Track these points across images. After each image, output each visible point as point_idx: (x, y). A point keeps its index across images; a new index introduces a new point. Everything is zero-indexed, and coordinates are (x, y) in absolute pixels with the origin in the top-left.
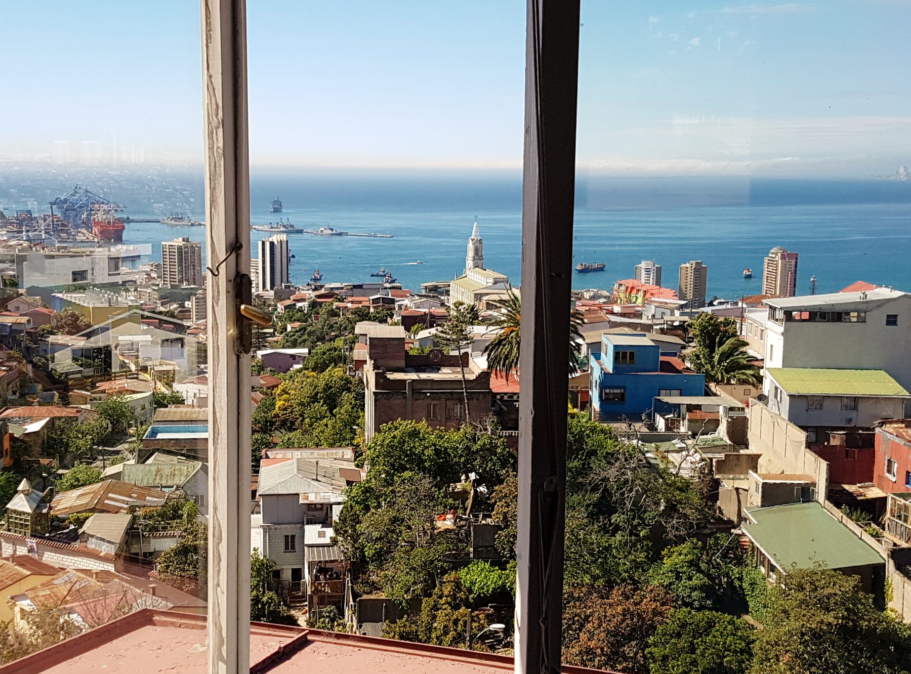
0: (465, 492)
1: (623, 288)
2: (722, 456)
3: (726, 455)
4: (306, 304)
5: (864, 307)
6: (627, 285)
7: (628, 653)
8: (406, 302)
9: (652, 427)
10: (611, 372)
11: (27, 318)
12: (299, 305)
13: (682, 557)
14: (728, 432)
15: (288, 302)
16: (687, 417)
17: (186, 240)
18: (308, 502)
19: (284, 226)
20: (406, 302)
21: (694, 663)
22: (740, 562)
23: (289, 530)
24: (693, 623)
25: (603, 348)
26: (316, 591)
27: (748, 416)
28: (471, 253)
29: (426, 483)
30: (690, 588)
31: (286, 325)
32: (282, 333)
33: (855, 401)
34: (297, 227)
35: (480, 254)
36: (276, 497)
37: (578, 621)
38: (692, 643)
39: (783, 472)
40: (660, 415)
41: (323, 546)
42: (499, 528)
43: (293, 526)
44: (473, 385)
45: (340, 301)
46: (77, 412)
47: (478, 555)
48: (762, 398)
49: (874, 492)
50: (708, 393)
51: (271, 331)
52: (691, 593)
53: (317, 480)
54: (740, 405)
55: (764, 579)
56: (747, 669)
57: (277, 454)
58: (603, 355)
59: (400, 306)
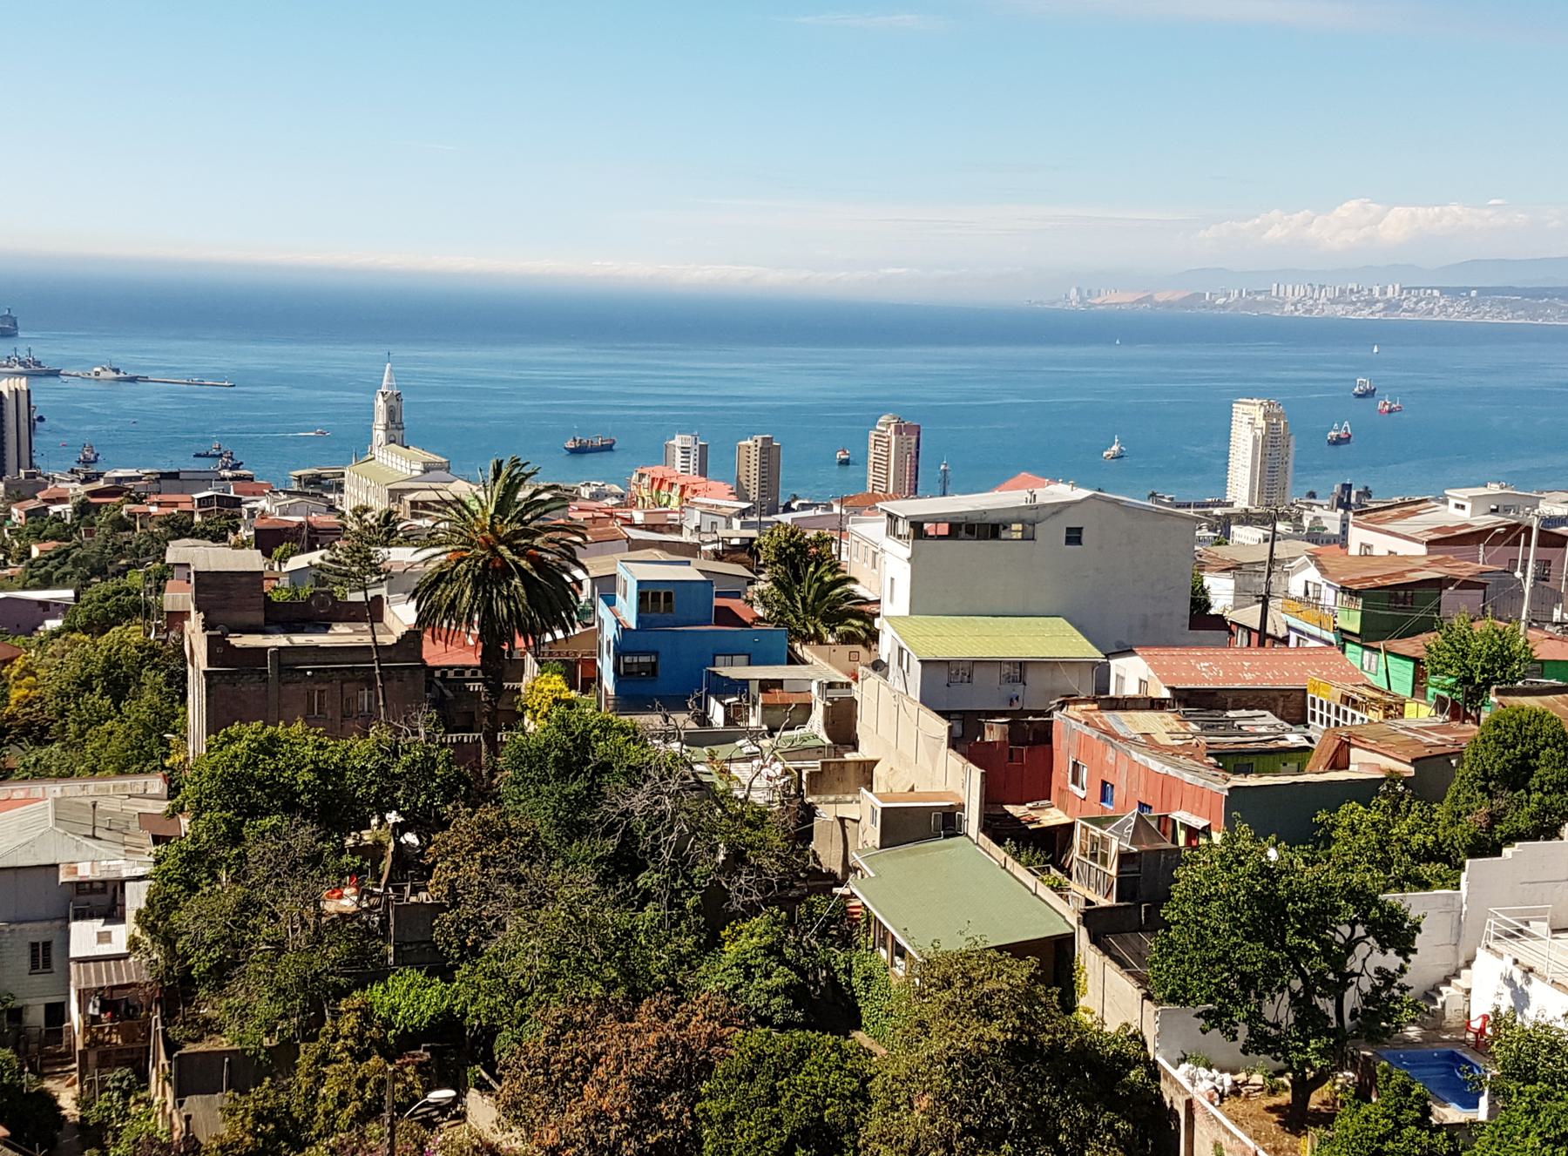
0: (379, 846)
1: (646, 481)
2: (817, 765)
3: (823, 763)
4: (68, 507)
5: (1029, 515)
6: (653, 475)
7: (667, 1114)
8: (263, 504)
9: (703, 719)
10: (634, 627)
12: (54, 509)
13: (755, 939)
14: (826, 724)
15: (32, 504)
16: (761, 701)
18: (77, 879)
19: (22, 364)
20: (263, 504)
21: (777, 1121)
22: (847, 942)
23: (37, 932)
24: (774, 1054)
25: (620, 585)
26: (93, 1043)
27: (857, 697)
28: (381, 419)
29: (305, 836)
30: (768, 992)
31: (29, 547)
32: (20, 561)
34: (47, 366)
36: (11, 872)
37: (581, 1063)
38: (773, 1088)
40: (717, 699)
41: (107, 958)
42: (439, 908)
43: (47, 924)
44: (392, 654)
45: (135, 502)
47: (403, 959)
48: (878, 666)
49: (1052, 817)
50: (793, 660)
52: (769, 1000)
53: (94, 837)
54: (845, 679)
55: (886, 969)
56: (862, 1124)
57: (13, 791)
58: (619, 597)
59: (252, 512)
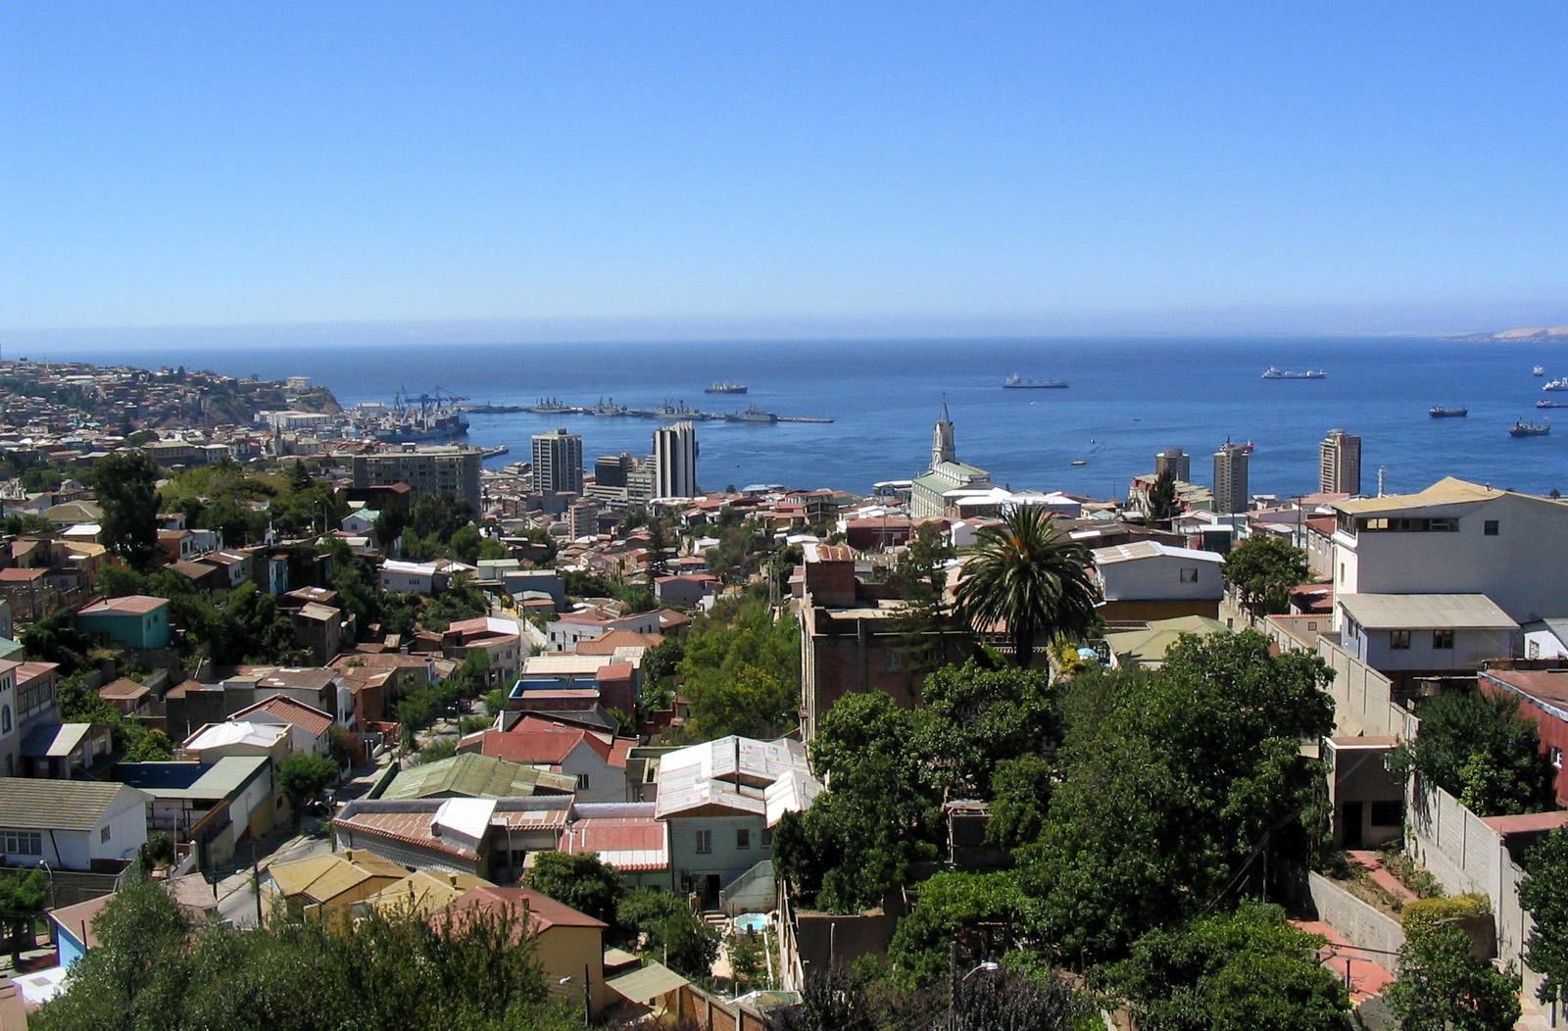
11: (366, 539)
17: (562, 432)
33: (1444, 638)
35: (951, 443)
39: (1361, 734)
46: (427, 660)
51: (674, 550)
